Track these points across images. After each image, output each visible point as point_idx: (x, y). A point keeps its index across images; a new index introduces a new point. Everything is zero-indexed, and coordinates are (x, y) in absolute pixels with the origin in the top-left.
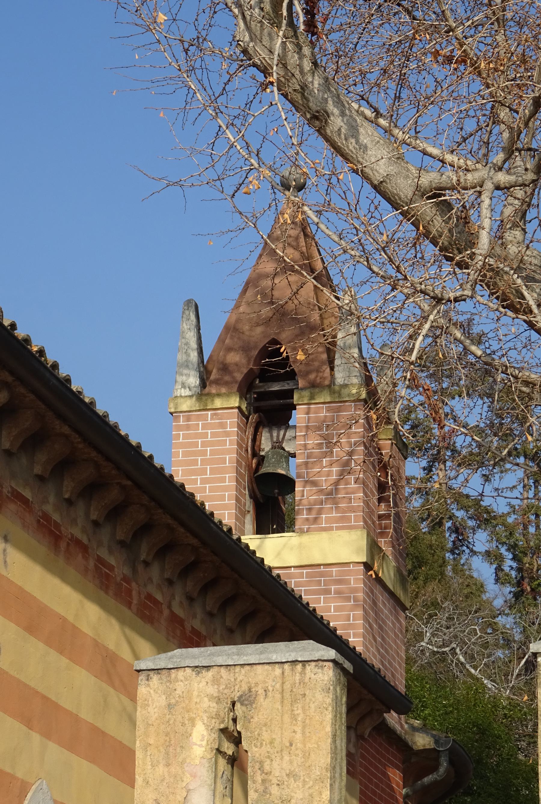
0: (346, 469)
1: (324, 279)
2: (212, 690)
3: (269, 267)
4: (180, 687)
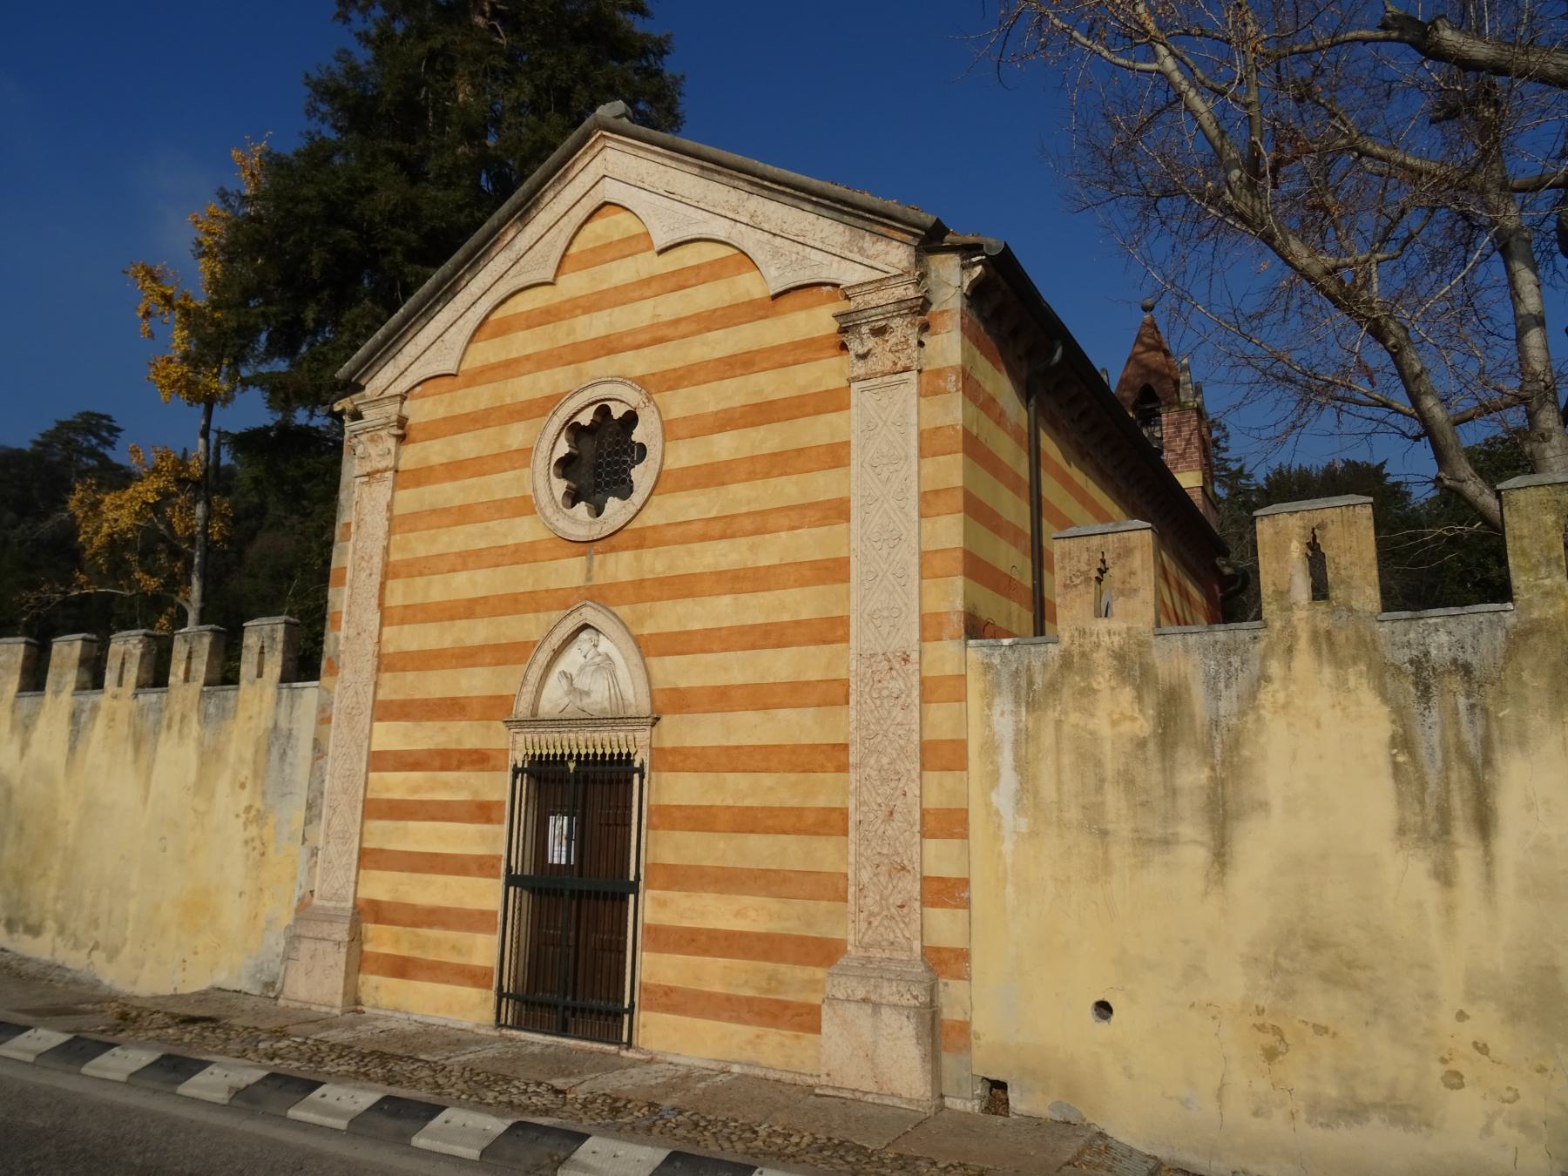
0: (1188, 442)
1: (1167, 353)
2: (1300, 523)
3: (1140, 349)
4: (1281, 523)
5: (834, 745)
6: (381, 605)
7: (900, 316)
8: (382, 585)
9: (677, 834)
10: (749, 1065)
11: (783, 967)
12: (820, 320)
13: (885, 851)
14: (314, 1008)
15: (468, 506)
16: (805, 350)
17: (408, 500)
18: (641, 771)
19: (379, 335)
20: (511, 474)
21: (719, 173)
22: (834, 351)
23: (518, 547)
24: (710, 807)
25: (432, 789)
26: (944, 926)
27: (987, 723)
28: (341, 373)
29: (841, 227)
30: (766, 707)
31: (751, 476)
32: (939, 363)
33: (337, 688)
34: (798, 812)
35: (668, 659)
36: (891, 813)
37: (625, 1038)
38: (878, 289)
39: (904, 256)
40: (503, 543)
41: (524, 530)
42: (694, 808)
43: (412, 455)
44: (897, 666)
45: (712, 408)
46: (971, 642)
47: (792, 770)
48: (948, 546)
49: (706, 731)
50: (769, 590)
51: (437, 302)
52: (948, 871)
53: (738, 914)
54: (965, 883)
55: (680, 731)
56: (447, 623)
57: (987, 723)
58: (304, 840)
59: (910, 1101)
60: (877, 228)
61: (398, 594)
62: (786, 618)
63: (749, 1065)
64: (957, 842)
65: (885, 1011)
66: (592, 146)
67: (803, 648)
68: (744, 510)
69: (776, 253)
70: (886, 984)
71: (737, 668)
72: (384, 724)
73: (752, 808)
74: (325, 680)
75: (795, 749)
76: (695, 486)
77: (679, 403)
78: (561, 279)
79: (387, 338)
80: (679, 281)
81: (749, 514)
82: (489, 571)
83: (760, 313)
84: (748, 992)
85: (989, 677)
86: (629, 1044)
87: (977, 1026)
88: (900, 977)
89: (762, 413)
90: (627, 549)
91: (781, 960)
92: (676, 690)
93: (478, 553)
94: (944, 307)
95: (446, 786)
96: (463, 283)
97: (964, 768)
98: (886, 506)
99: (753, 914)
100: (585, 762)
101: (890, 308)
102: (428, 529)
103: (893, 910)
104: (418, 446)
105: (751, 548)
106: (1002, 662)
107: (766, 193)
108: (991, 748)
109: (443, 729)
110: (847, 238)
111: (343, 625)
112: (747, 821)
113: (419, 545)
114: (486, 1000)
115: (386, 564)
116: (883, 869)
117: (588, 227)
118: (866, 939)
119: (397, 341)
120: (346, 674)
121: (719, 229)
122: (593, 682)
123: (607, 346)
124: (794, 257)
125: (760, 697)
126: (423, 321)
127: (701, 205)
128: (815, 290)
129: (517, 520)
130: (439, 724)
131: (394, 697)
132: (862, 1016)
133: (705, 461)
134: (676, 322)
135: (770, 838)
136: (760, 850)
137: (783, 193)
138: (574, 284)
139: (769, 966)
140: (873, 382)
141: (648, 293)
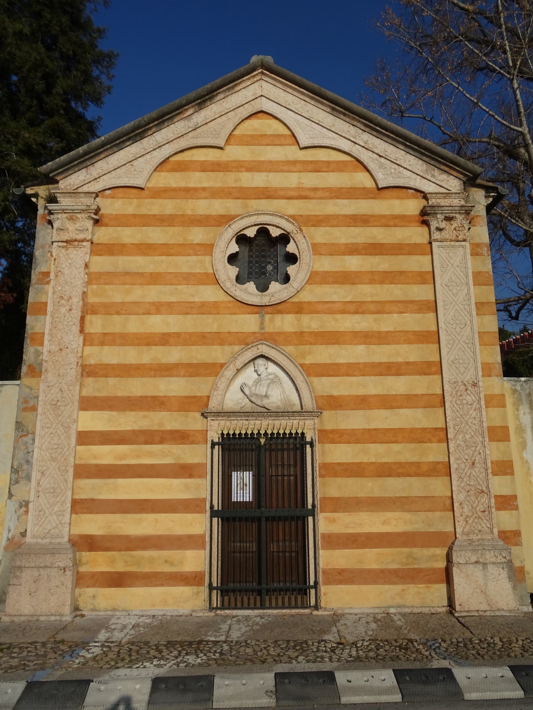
5: (436, 429)
6: (82, 331)
7: (459, 213)
8: (82, 319)
9: (339, 480)
10: (399, 607)
11: (415, 550)
12: (412, 206)
13: (472, 483)
14: (42, 619)
15: (159, 274)
16: (400, 220)
17: (102, 263)
18: (312, 444)
19: (81, 150)
20: (195, 258)
21: (345, 115)
22: (418, 224)
23: (203, 304)
24: (360, 463)
25: (138, 457)
26: (505, 520)
27: (517, 417)
28: (43, 169)
29: (420, 162)
30: (391, 408)
31: (372, 282)
32: (477, 240)
33: (42, 386)
34: (418, 464)
35: (324, 379)
36: (473, 464)
37: (313, 602)
38: (445, 198)
39: (457, 184)
40: (191, 300)
41: (209, 294)
42: (349, 464)
43: (103, 235)
44: (470, 388)
45: (343, 241)
46: (505, 378)
47: (411, 442)
48: (491, 330)
49: (355, 420)
50: (388, 344)
51: (128, 140)
52: (506, 492)
53: (384, 523)
54: (515, 497)
55: (333, 420)
56: (145, 348)
57: (517, 417)
58: (10, 495)
59: (510, 611)
60: (442, 167)
61: (96, 324)
62: (400, 360)
63: (399, 607)
64: (509, 477)
65: (490, 567)
66: (254, 76)
67: (412, 377)
68: (369, 299)
69: (381, 166)
70: (487, 552)
71: (372, 386)
72: (89, 413)
73: (388, 463)
74: (26, 380)
75: (412, 431)
76: (335, 282)
77: (321, 235)
78: (228, 148)
79: (86, 154)
80: (317, 167)
81: (372, 302)
82: (181, 317)
83: (371, 195)
84: (395, 566)
85: (516, 396)
86: (317, 607)
87: (527, 569)
88: (494, 548)
89: (375, 249)
90: (290, 313)
91: (415, 546)
92: (332, 396)
93: (170, 305)
94: (477, 214)
95: (151, 454)
96: (150, 132)
97: (509, 440)
98: (457, 307)
99: (394, 522)
100: (272, 438)
101: (457, 208)
102: (123, 284)
103: (480, 514)
104: (110, 229)
105: (375, 321)
106: (521, 389)
107: (375, 133)
108: (520, 430)
109: (145, 417)
110: (425, 168)
111: (46, 342)
112: (385, 470)
113: (116, 294)
114: (198, 593)
115: (85, 304)
116: (472, 493)
117: (248, 122)
118: (466, 530)
119: (92, 157)
120: (50, 377)
121: (345, 145)
122: (260, 389)
123: (266, 194)
124: (393, 171)
125: (388, 402)
126: (115, 149)
127: (333, 129)
128: (404, 190)
129: (202, 287)
130: (141, 414)
131: (98, 394)
132: (477, 571)
133: (341, 269)
134: (315, 189)
135: (401, 480)
136: (395, 486)
137: (388, 136)
138: (236, 153)
139: (406, 550)
140: (445, 243)
141: (295, 169)
